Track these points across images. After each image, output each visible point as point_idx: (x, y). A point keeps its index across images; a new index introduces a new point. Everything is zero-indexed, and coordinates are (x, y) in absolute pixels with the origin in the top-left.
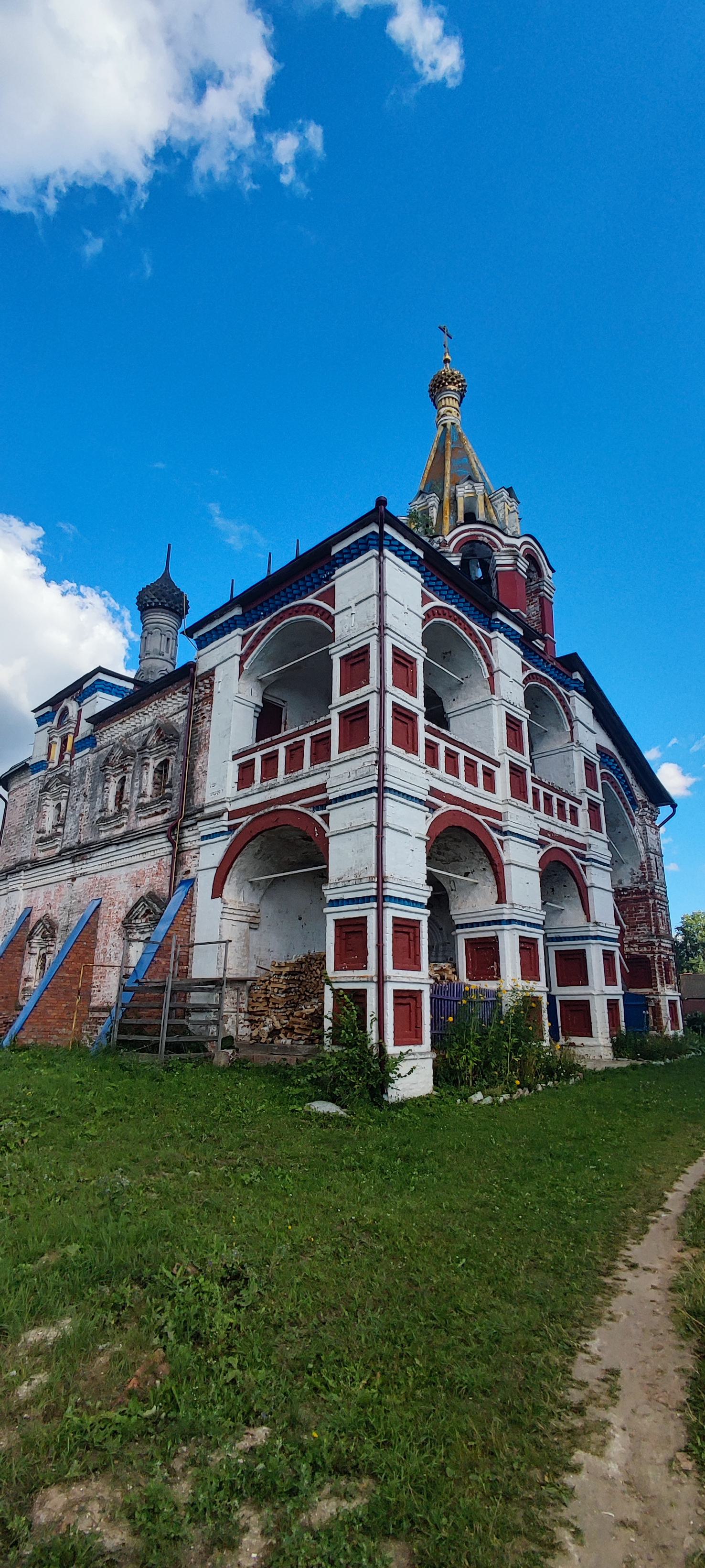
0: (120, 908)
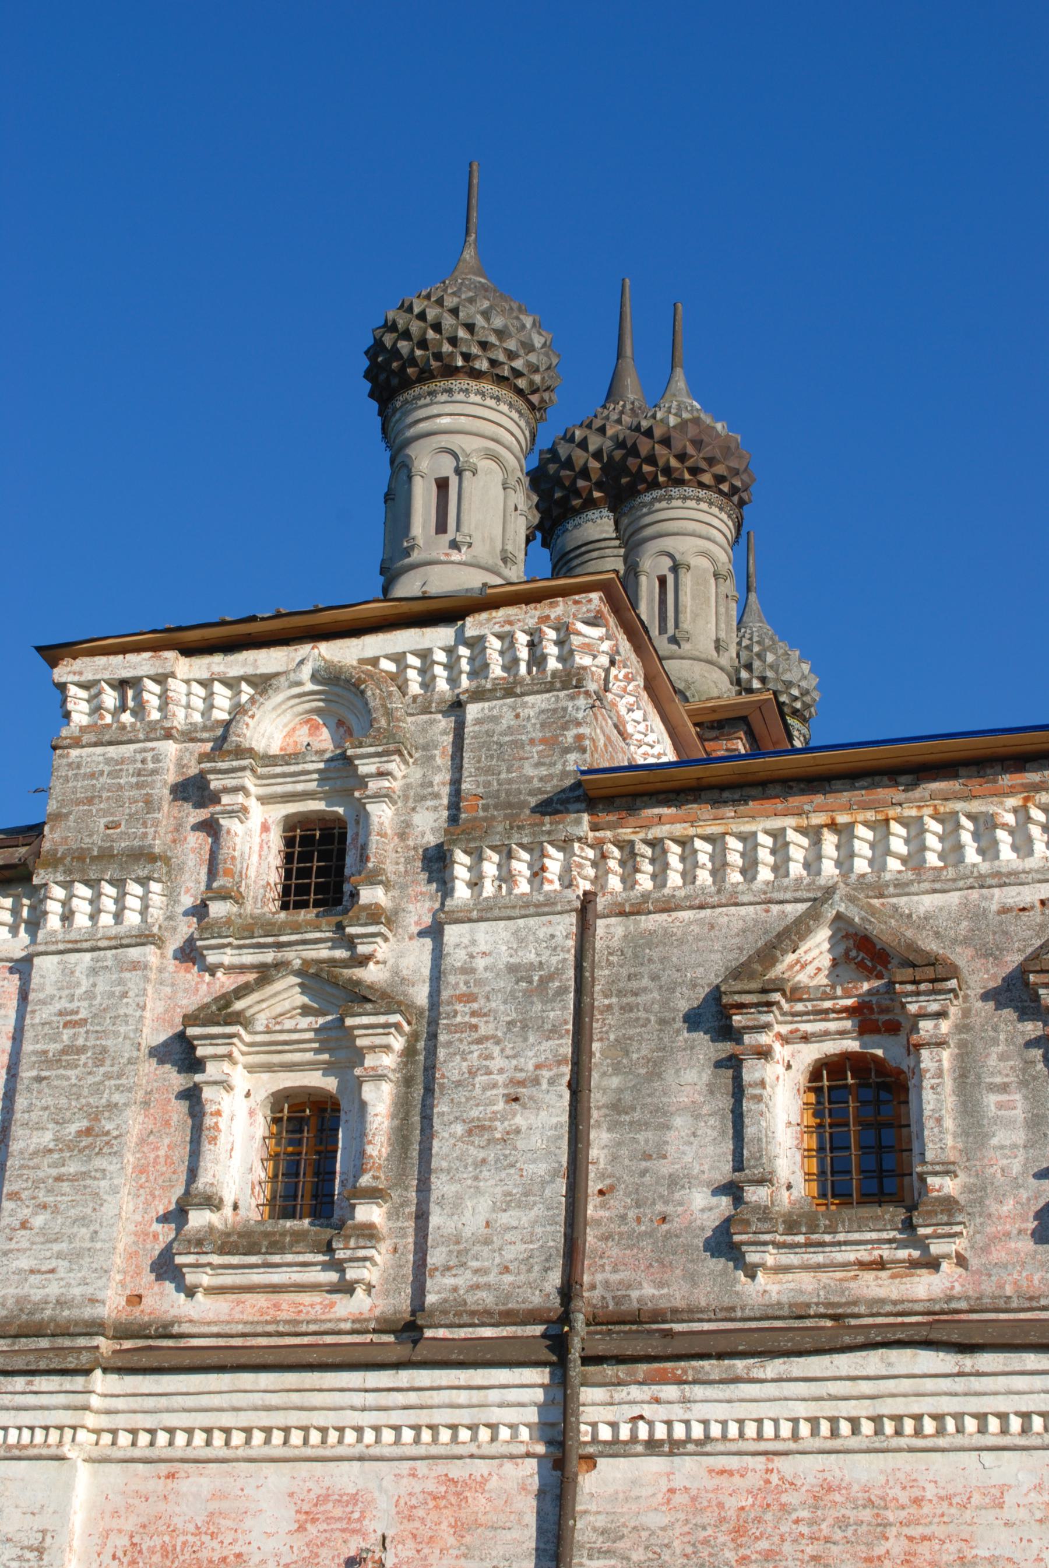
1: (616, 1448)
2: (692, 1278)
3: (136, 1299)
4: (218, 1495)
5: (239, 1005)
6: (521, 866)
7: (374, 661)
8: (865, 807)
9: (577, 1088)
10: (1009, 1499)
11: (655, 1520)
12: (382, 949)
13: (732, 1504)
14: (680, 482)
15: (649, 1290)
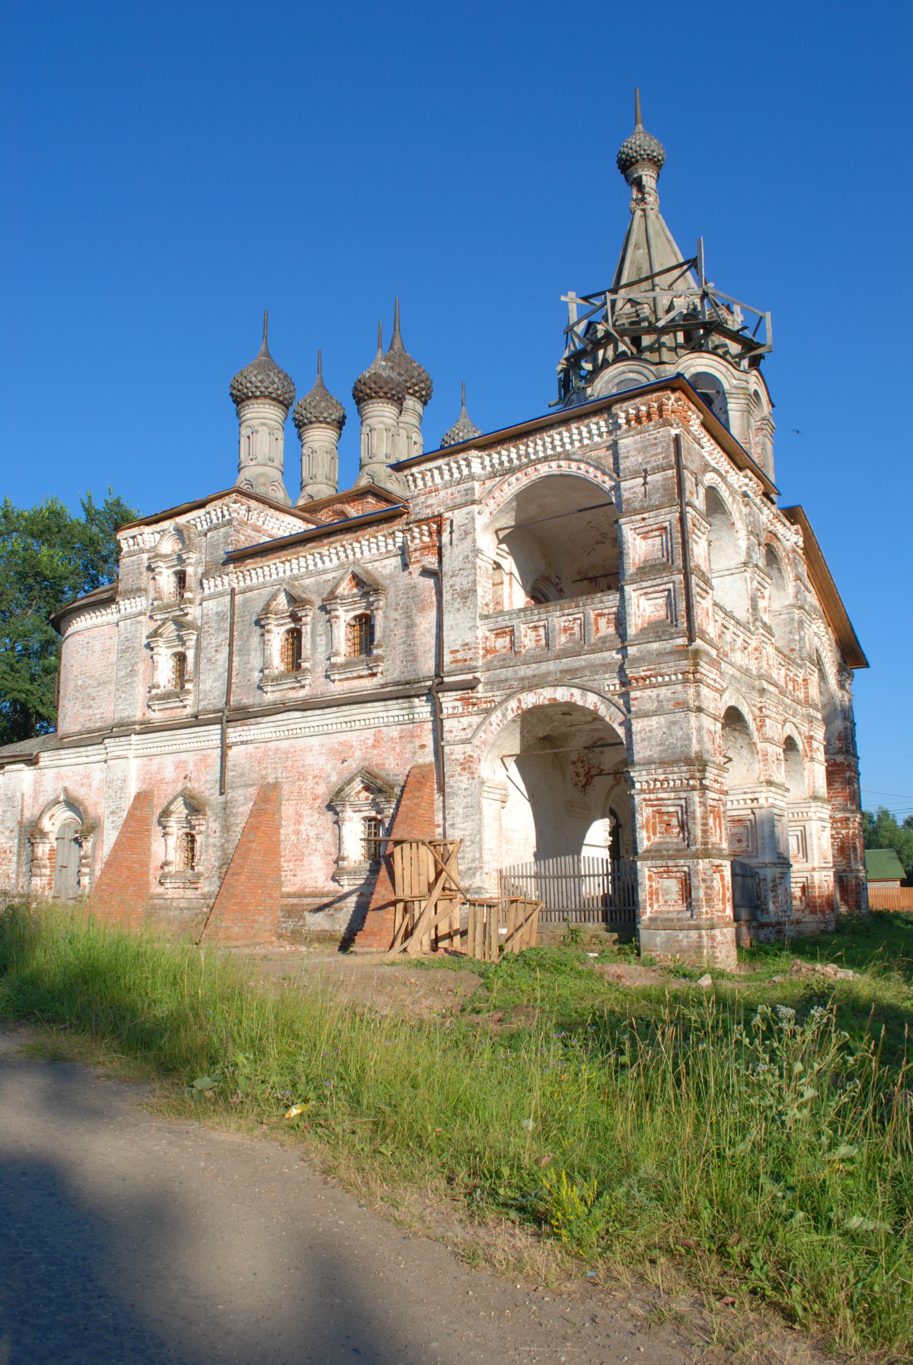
0: (317, 783)
1: (235, 744)
2: (254, 696)
3: (144, 714)
4: (160, 764)
5: (160, 631)
6: (219, 582)
7: (188, 522)
8: (294, 553)
9: (231, 645)
10: (314, 748)
11: (243, 761)
12: (190, 610)
13: (259, 755)
14: (372, 398)
15: (245, 701)
